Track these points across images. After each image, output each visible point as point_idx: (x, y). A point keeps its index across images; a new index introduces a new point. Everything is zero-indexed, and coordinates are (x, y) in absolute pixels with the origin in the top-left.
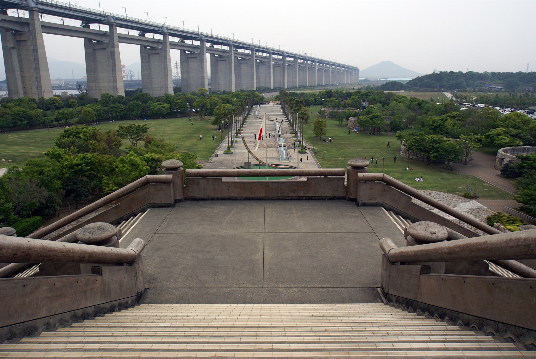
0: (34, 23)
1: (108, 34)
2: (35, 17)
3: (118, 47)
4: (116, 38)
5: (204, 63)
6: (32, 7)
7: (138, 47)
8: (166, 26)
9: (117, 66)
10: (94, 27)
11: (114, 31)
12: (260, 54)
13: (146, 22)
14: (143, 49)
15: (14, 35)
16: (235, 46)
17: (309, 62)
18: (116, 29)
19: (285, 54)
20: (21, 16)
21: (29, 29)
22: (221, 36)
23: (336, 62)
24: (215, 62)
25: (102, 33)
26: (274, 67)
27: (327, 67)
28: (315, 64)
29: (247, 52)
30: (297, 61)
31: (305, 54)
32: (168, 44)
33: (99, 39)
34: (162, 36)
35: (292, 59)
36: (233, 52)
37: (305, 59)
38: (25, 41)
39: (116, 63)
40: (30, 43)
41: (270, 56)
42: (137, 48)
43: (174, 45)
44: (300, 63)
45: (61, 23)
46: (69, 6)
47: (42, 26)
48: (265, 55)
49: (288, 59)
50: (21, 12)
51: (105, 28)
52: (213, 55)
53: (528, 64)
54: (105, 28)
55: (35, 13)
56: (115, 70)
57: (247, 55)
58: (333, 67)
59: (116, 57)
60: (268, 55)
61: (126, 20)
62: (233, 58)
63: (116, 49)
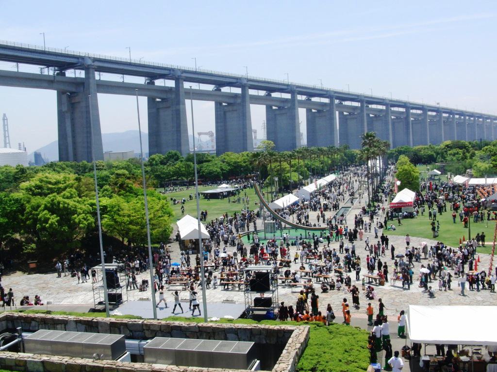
0: (89, 81)
1: (174, 90)
2: (91, 75)
3: (185, 104)
4: (182, 93)
5: (295, 119)
6: (89, 65)
7: (264, 107)
8: (246, 77)
9: (182, 127)
10: (159, 83)
11: (181, 85)
12: (374, 106)
13: (320, 88)
14: (219, 106)
15: (69, 97)
16: (477, 117)
17: (457, 116)
18: (183, 84)
19: (409, 105)
20: (78, 76)
21: (84, 88)
22: (318, 85)
23: (483, 113)
24: (343, 118)
25: (167, 89)
26: (412, 124)
27: (480, 121)
28: (465, 118)
29: (380, 107)
30: (427, 114)
31: (438, 104)
32: (296, 103)
33: (164, 96)
34: (290, 95)
35: (434, 114)
36: (365, 107)
37: (438, 110)
38: (79, 102)
39: (182, 123)
40: (83, 104)
41: (293, 97)
42: (210, 105)
43: (257, 100)
44: (445, 117)
45: (121, 80)
46: (129, 61)
47: (97, 85)
48: (380, 107)
49: (430, 113)
50: (78, 71)
51: (171, 84)
52: (309, 111)
53: (481, 140)
54: (171, 84)
55: (91, 71)
56: (180, 131)
57: (355, 108)
58: (481, 120)
59: (181, 116)
60: (384, 108)
61: (195, 73)
62: (365, 115)
63: (181, 106)
